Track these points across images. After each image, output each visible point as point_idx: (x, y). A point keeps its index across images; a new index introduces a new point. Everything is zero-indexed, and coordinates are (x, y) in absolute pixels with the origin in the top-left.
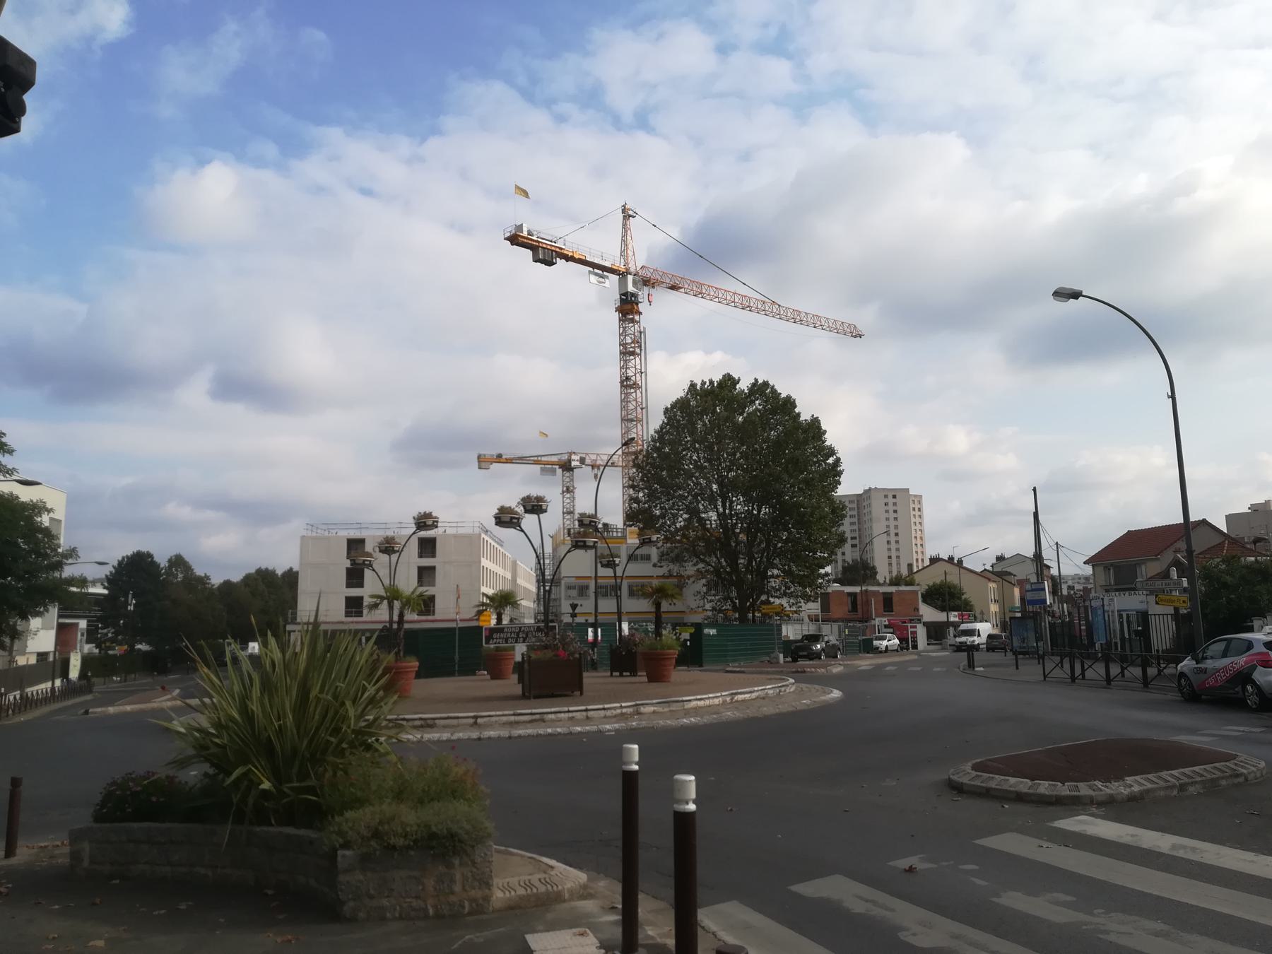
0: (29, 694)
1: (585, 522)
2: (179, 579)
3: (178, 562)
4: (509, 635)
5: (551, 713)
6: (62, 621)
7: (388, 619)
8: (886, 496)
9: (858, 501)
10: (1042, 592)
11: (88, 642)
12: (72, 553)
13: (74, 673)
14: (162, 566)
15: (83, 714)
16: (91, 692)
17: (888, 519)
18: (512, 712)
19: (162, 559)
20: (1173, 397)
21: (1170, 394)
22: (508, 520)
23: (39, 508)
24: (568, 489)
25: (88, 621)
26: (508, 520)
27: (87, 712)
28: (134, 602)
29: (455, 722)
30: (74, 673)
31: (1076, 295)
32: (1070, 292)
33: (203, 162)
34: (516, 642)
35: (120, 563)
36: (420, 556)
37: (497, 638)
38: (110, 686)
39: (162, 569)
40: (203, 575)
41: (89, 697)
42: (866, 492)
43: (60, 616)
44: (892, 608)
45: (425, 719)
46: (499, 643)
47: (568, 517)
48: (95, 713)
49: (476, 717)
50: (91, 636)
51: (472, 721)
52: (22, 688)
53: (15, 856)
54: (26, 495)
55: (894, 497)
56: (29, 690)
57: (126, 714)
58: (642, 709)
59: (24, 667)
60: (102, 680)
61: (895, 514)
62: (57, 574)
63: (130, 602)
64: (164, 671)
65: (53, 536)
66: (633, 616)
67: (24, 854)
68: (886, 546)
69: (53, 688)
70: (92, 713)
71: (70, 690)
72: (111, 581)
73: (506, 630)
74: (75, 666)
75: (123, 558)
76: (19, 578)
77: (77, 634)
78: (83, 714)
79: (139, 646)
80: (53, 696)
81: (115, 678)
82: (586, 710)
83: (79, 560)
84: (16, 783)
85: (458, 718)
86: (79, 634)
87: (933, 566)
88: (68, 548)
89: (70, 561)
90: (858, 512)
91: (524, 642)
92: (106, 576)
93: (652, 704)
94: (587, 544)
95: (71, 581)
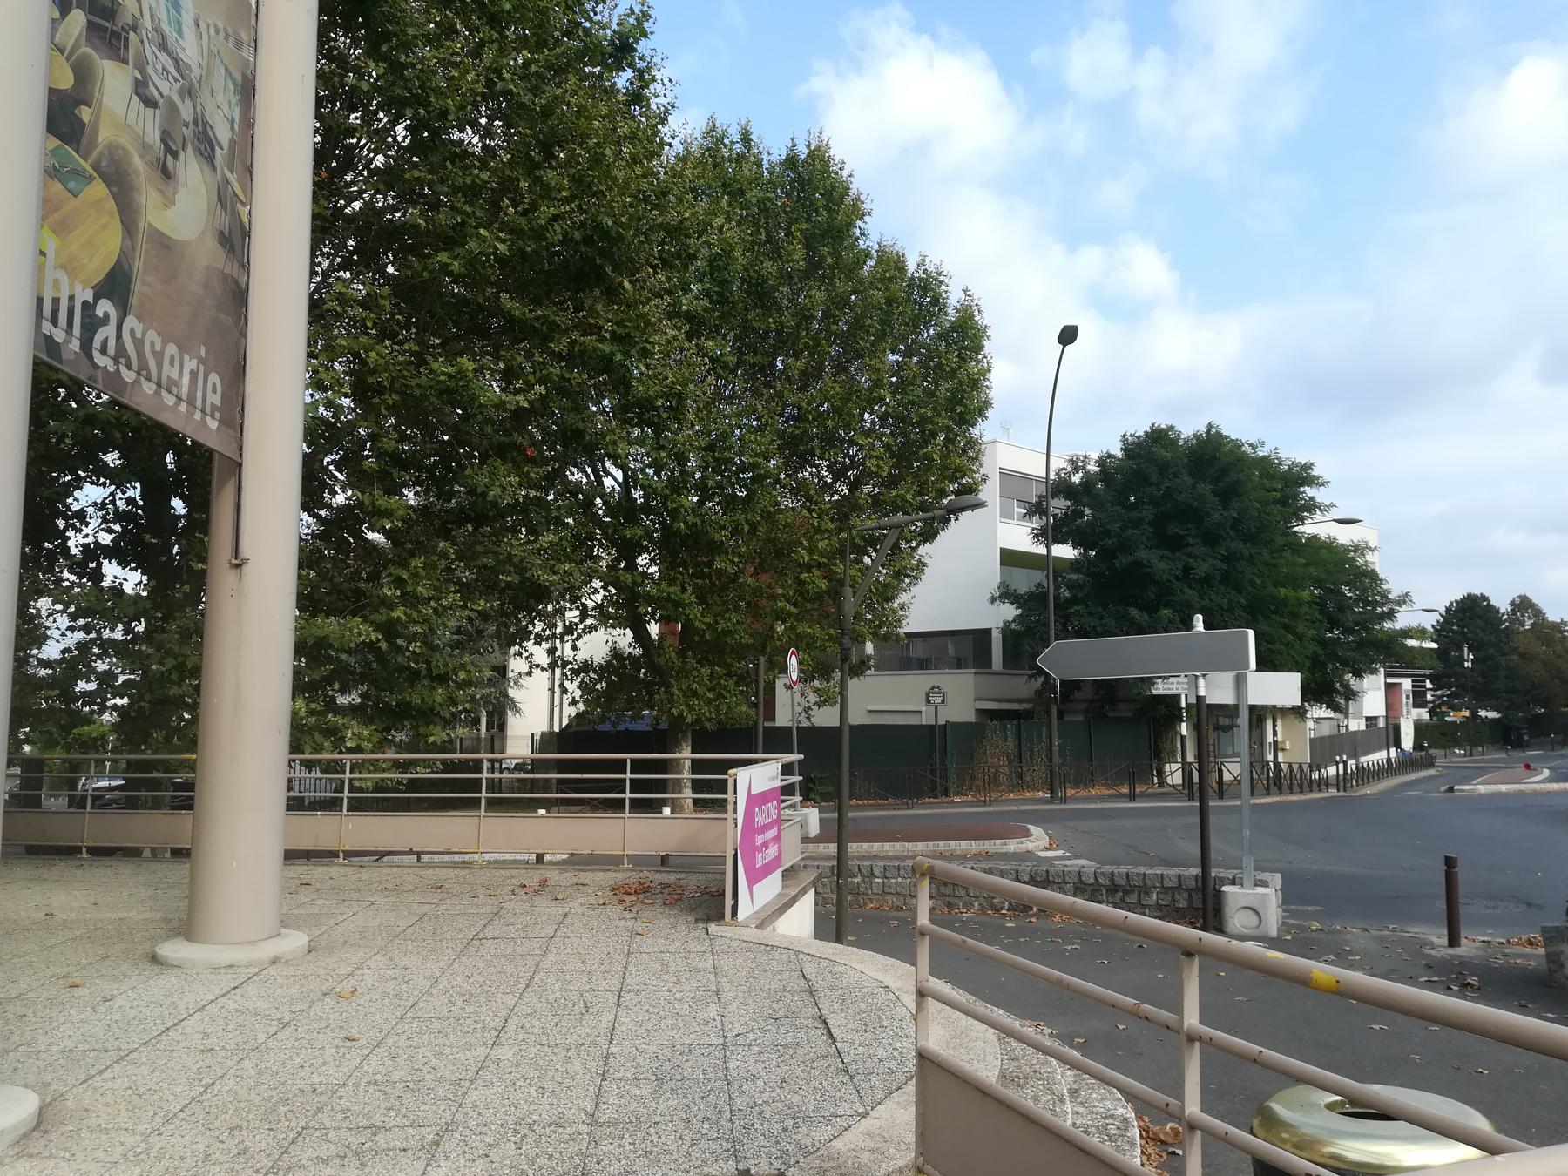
0: (1365, 765)
2: (1527, 627)
3: (1523, 605)
6: (1389, 681)
11: (1416, 705)
12: (1404, 599)
13: (1407, 742)
14: (1502, 611)
15: (1445, 792)
16: (1432, 765)
19: (1502, 602)
23: (1359, 549)
25: (1413, 681)
27: (1451, 789)
28: (1472, 657)
30: (1407, 742)
33: (1505, 67)
35: (1448, 610)
38: (1453, 760)
39: (1503, 615)
40: (1559, 621)
41: (1432, 772)
43: (1387, 676)
48: (1462, 791)
50: (1418, 699)
52: (1356, 756)
53: (1459, 946)
54: (1344, 536)
56: (1364, 759)
57: (1500, 794)
59: (1355, 732)
60: (1442, 752)
62: (1388, 625)
64: (1519, 745)
65: (1381, 580)
66: (1254, 723)
67: (1468, 947)
69: (1389, 759)
70: (1458, 790)
71: (1406, 764)
72: (1440, 632)
74: (1407, 734)
75: (1451, 603)
76: (1347, 631)
78: (1445, 792)
79: (1482, 713)
80: (1389, 769)
81: (1457, 751)
83: (1415, 607)
84: (1450, 863)
86: (1404, 696)
88: (1400, 594)
89: (1404, 608)
95: (1407, 633)
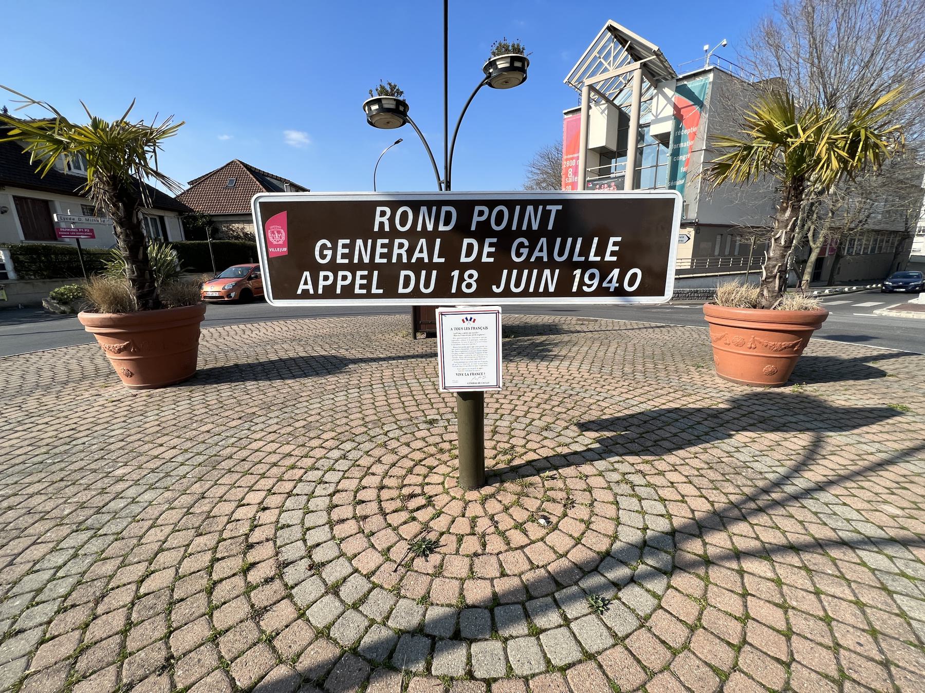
4: (400, 250)
34: (442, 291)
37: (333, 267)
46: (348, 292)
73: (380, 219)
91: (484, 291)
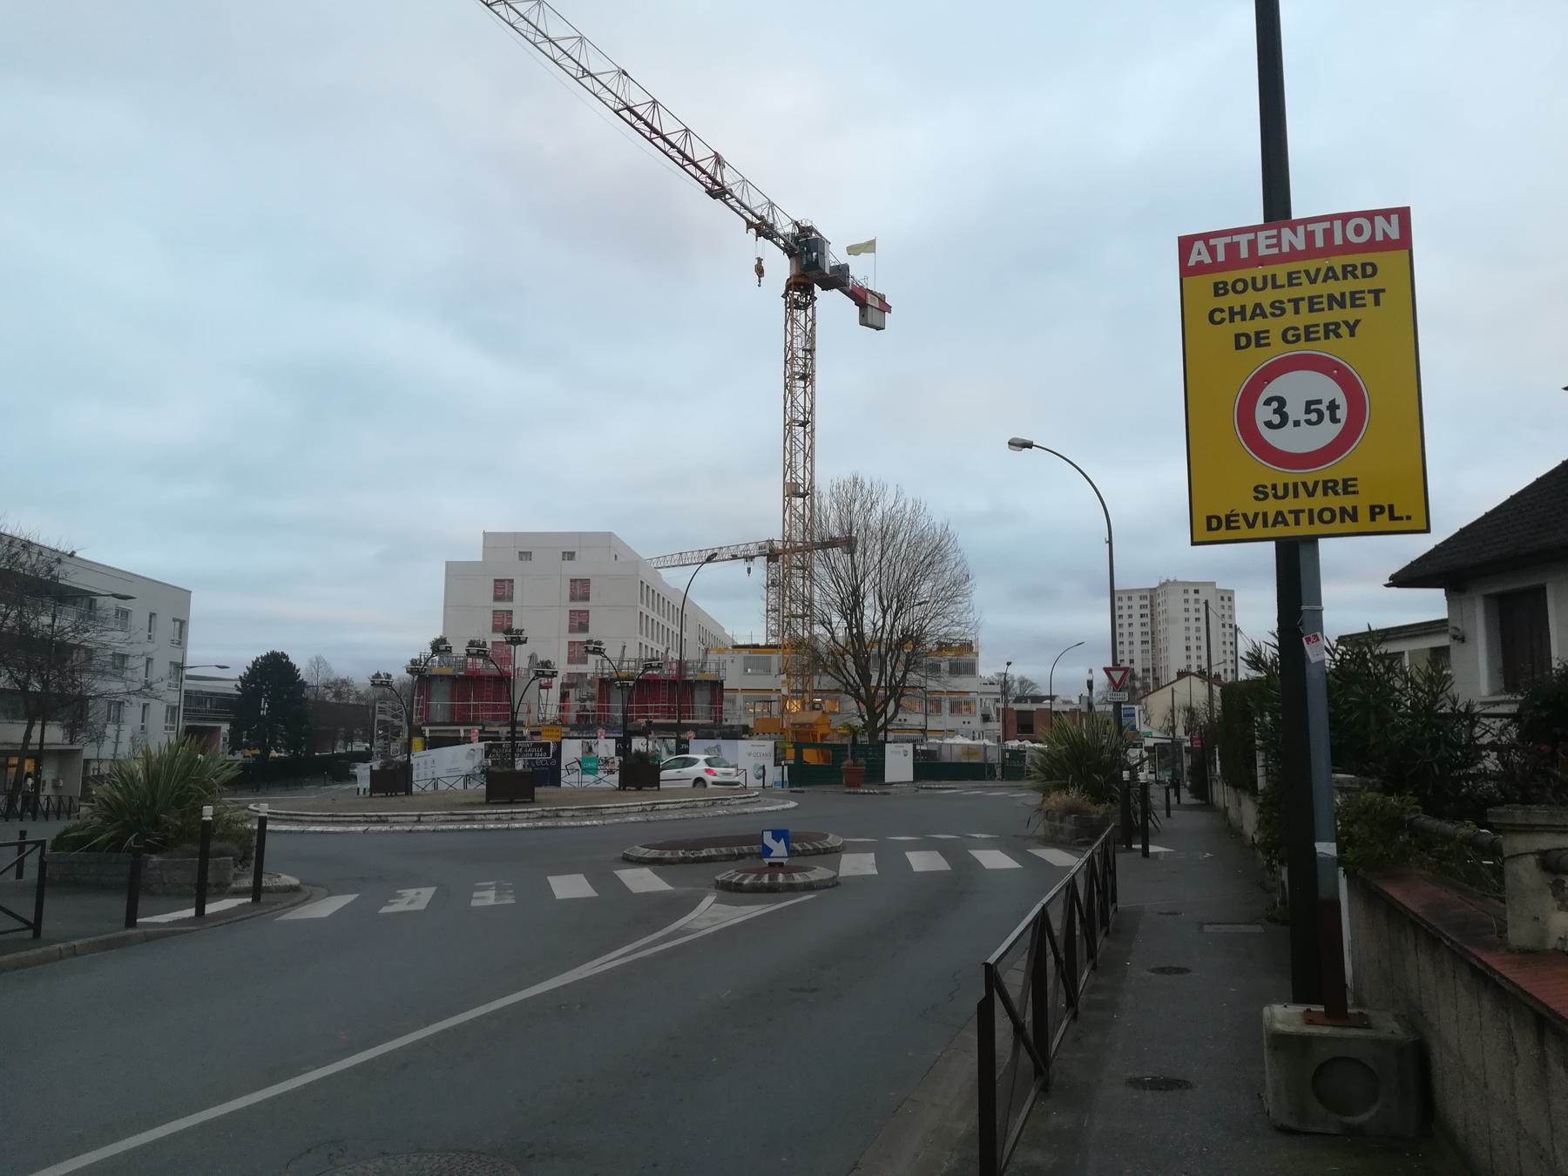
1: (589, 649)
5: (481, 814)
7: (39, 741)
8: (1186, 591)
9: (1151, 597)
10: (1132, 718)
17: (1187, 620)
18: (449, 812)
20: (1110, 542)
21: (1107, 539)
22: (475, 652)
24: (773, 583)
26: (475, 652)
29: (403, 819)
31: (1029, 445)
32: (1021, 442)
36: (511, 612)
42: (1162, 585)
44: (1032, 729)
45: (380, 816)
47: (774, 615)
49: (419, 816)
51: (416, 818)
55: (1196, 592)
58: (561, 813)
61: (1198, 616)
63: (262, 706)
68: (1185, 653)
75: (258, 659)
77: (219, 738)
82: (512, 813)
85: (406, 816)
86: (222, 739)
87: (1180, 681)
90: (1152, 610)
92: (240, 677)
93: (573, 810)
94: (546, 673)
